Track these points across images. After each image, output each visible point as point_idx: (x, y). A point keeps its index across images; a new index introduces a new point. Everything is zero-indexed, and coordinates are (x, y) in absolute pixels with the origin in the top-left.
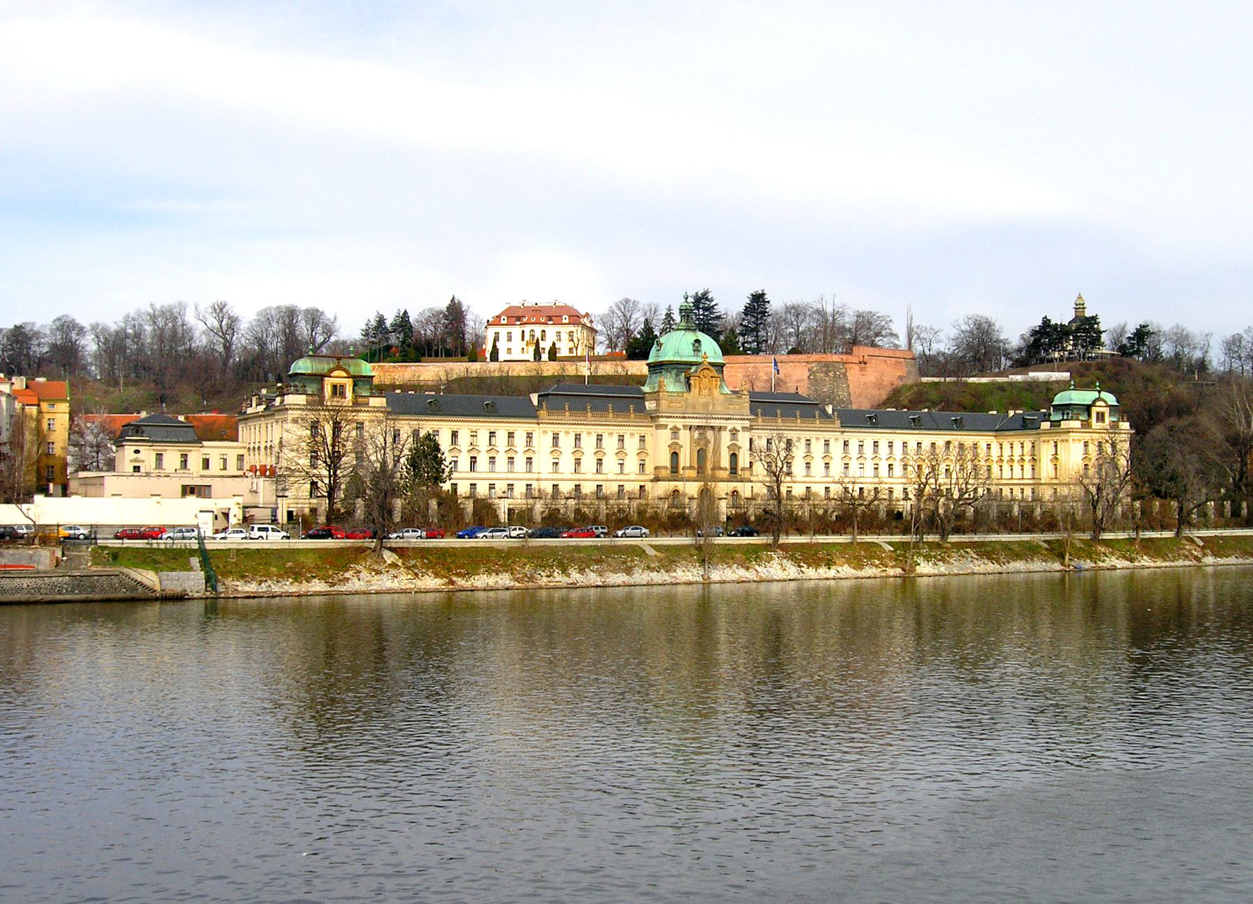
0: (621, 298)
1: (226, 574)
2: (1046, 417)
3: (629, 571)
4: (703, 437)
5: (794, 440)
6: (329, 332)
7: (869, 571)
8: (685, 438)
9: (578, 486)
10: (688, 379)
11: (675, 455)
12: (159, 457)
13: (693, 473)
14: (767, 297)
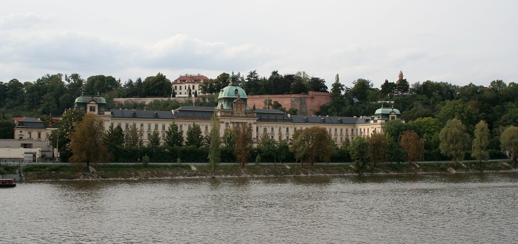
2: (373, 119)
5: (267, 127)
12: (39, 134)
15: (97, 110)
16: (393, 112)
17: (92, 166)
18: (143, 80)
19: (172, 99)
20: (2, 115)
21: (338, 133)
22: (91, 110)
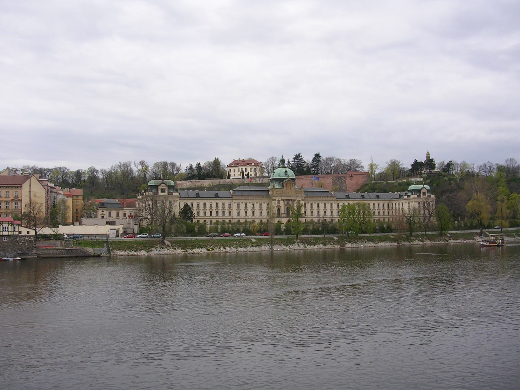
0: (271, 156)
1: (113, 249)
2: (406, 194)
3: (246, 247)
4: (288, 203)
6: (178, 170)
7: (329, 246)
8: (282, 204)
9: (239, 221)
10: (283, 184)
11: (279, 210)
12: (110, 213)
13: (285, 215)
14: (320, 155)
15: (166, 192)
16: (424, 188)
17: (168, 241)
18: (202, 165)
19: (227, 180)
20: (3, 206)
21: (379, 208)
22: (162, 192)
